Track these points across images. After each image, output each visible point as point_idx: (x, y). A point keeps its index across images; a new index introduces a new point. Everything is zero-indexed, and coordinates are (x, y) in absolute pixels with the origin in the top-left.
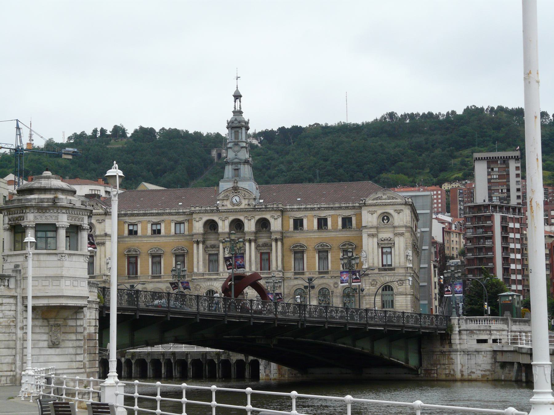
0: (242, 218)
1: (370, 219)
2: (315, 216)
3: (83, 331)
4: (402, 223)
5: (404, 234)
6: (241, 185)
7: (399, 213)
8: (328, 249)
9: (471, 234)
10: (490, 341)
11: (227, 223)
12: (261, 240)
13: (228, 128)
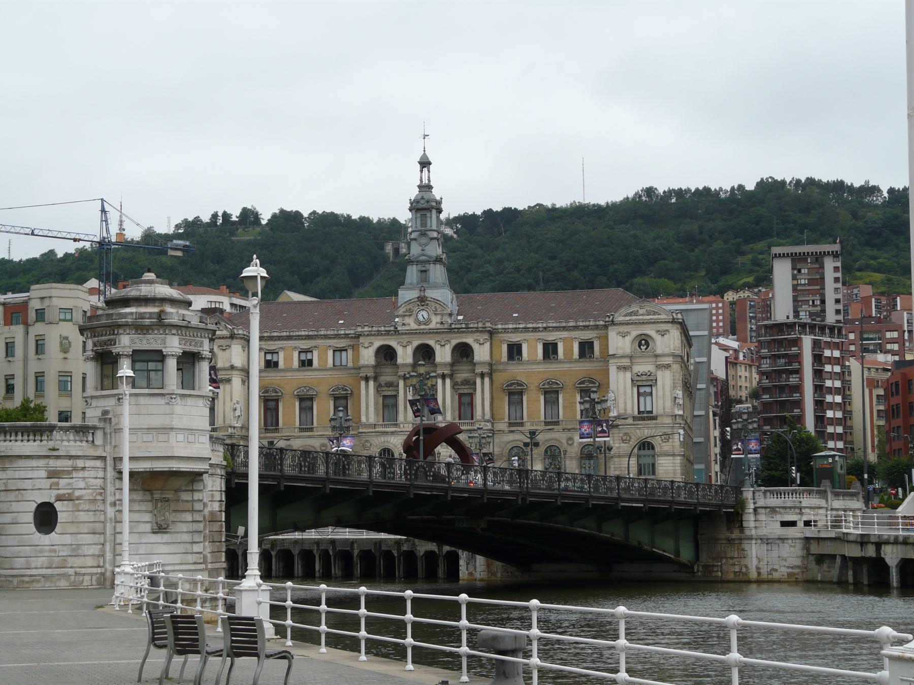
0: (431, 343)
1: (620, 344)
2: (539, 339)
3: (202, 509)
4: (668, 349)
6: (430, 294)
7: (663, 335)
9: (767, 366)
10: (801, 524)
11: (410, 350)
12: (459, 375)
13: (410, 210)
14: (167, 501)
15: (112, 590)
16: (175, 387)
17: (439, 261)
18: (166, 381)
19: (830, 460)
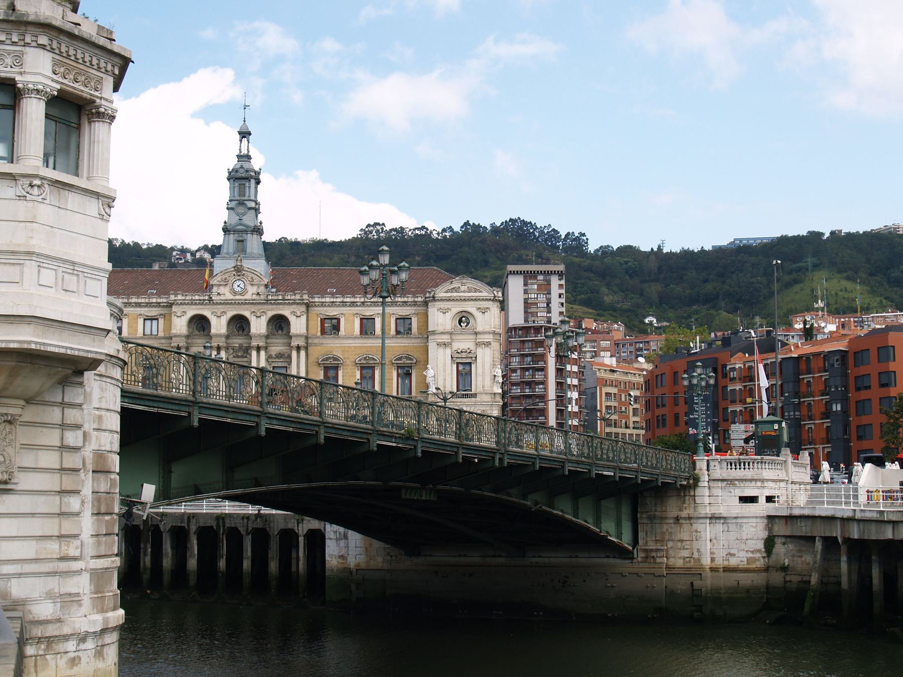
0: (247, 314)
2: (357, 314)
3: (80, 444)
4: (488, 327)
5: (490, 344)
6: (247, 264)
8: (375, 363)
9: (516, 364)
10: (762, 500)
11: (224, 320)
12: (274, 348)
13: (229, 179)
14: (10, 422)
15: (46, 152)
16: (40, 163)
17: (257, 232)
18: (20, 149)
19: (776, 427)
